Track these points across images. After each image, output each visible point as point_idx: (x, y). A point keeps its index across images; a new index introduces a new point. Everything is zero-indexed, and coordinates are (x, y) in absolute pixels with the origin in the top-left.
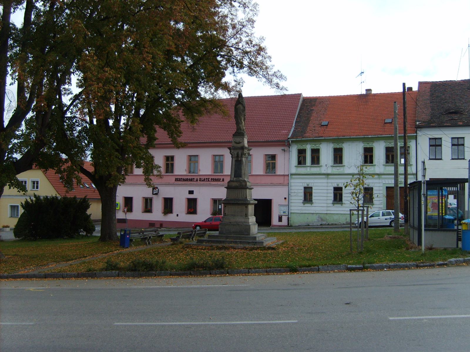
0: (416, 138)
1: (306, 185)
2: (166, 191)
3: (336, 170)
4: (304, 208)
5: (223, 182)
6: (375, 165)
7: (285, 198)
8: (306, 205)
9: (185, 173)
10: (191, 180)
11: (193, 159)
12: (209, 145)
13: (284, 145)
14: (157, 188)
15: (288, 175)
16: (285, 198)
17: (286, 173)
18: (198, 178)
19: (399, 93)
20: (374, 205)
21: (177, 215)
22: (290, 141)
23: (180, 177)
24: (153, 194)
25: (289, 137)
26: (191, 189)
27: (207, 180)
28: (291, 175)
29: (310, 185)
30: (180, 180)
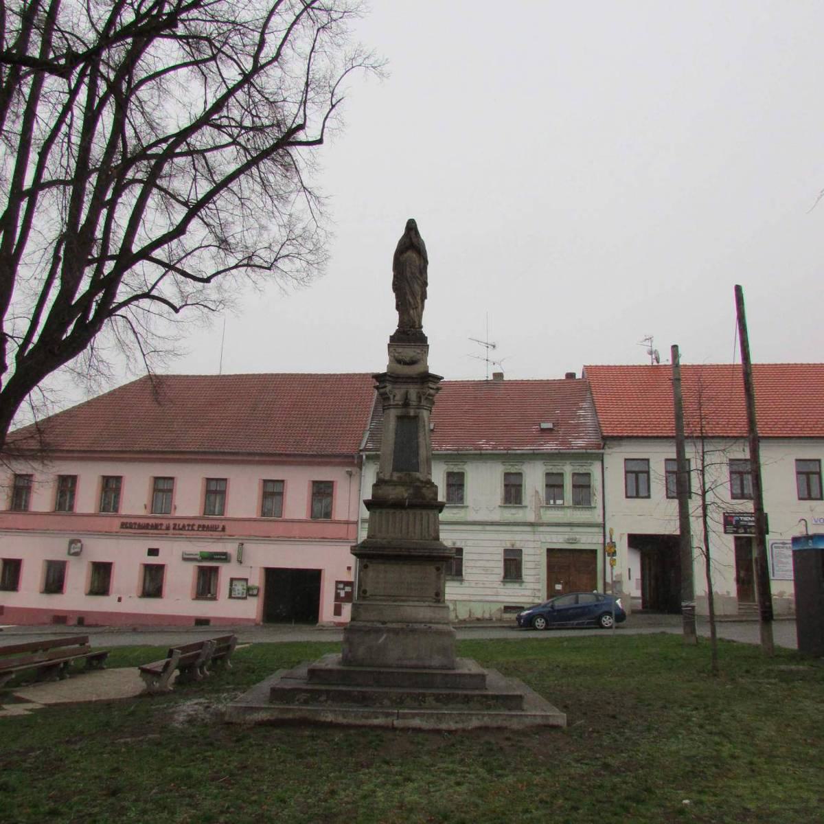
0: (603, 457)
1: (508, 546)
2: (100, 550)
3: (451, 515)
4: (502, 591)
5: (222, 533)
6: (526, 507)
7: (349, 568)
8: (509, 585)
9: (142, 512)
10: (156, 527)
11: (161, 485)
12: (115, 456)
13: (352, 464)
14: (80, 541)
15: (356, 523)
16: (349, 568)
17: (353, 519)
18: (172, 523)
19: (536, 382)
20: (524, 584)
21: (120, 600)
22: (364, 457)
23: (133, 521)
24: (69, 554)
25: (361, 448)
26: (154, 545)
27: (190, 528)
28: (362, 522)
29: (518, 546)
30: (133, 527)
